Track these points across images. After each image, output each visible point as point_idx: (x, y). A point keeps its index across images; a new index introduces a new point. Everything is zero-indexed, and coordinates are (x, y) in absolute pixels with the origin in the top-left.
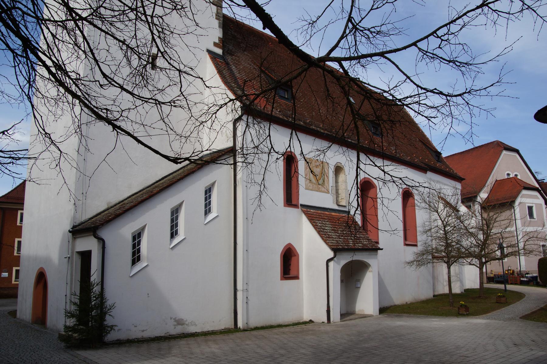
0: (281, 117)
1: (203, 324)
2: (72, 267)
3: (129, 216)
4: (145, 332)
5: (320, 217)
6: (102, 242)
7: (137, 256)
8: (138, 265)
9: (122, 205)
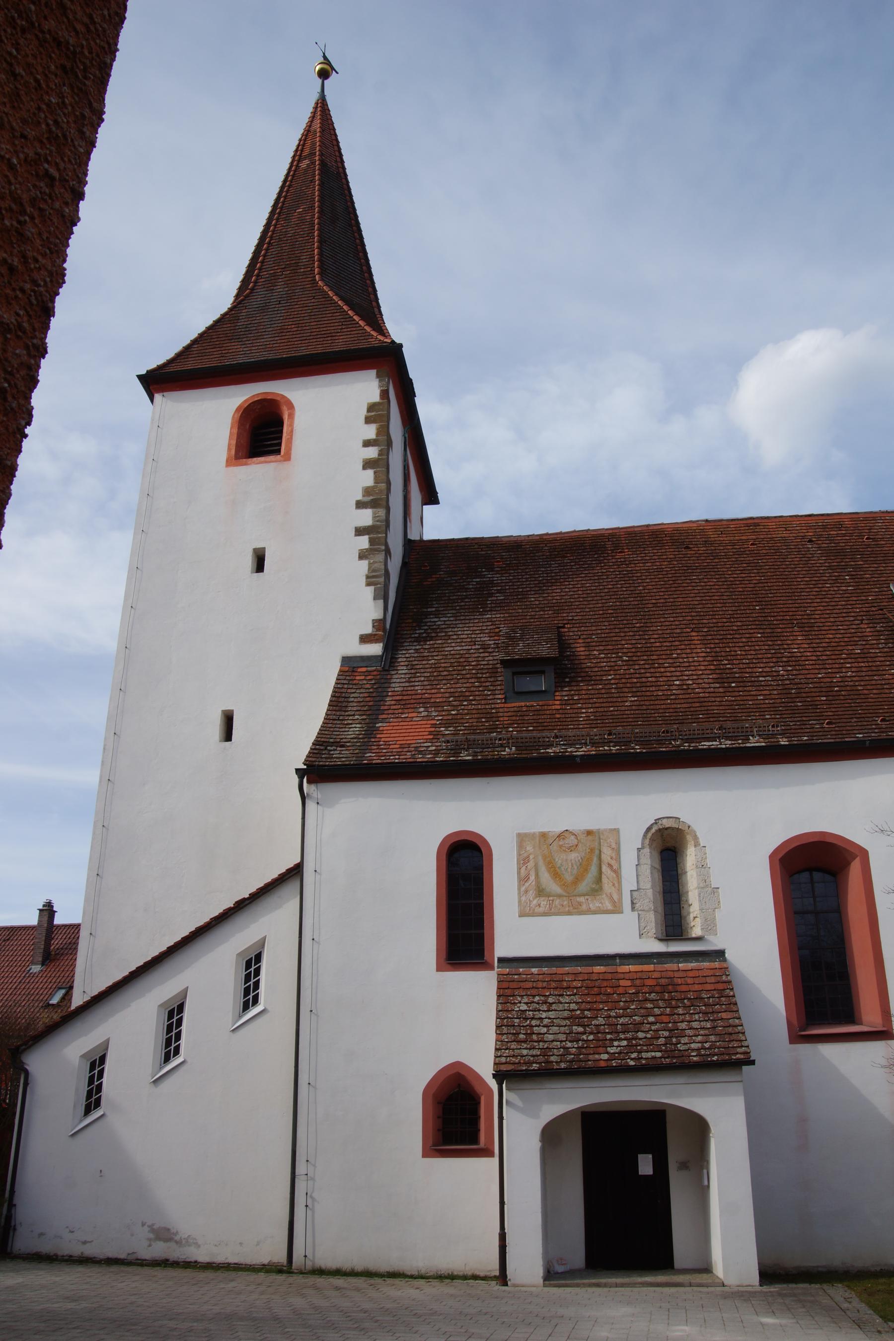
1: (216, 1245)
4: (88, 1244)
7: (94, 1098)
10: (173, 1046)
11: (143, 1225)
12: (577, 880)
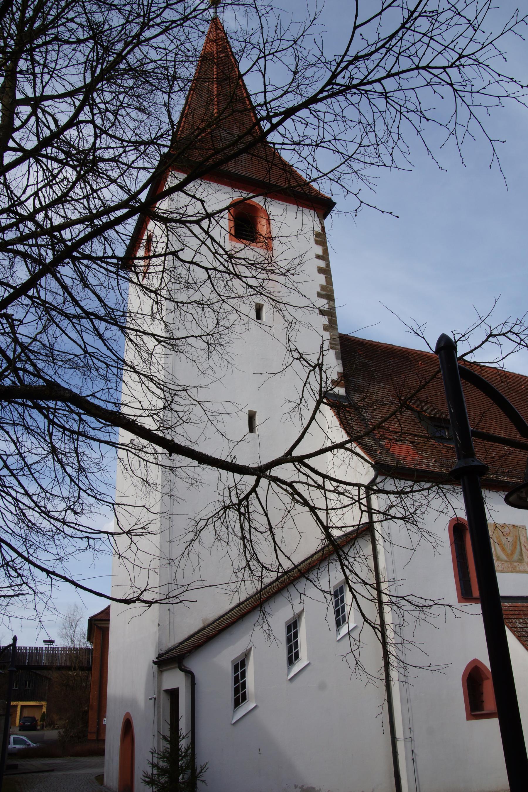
0: (436, 470)
2: (159, 713)
3: (226, 637)
5: (521, 613)
6: (190, 675)
7: (241, 693)
8: (243, 706)
9: (221, 622)
10: (294, 652)
11: (296, 787)
12: (513, 553)
